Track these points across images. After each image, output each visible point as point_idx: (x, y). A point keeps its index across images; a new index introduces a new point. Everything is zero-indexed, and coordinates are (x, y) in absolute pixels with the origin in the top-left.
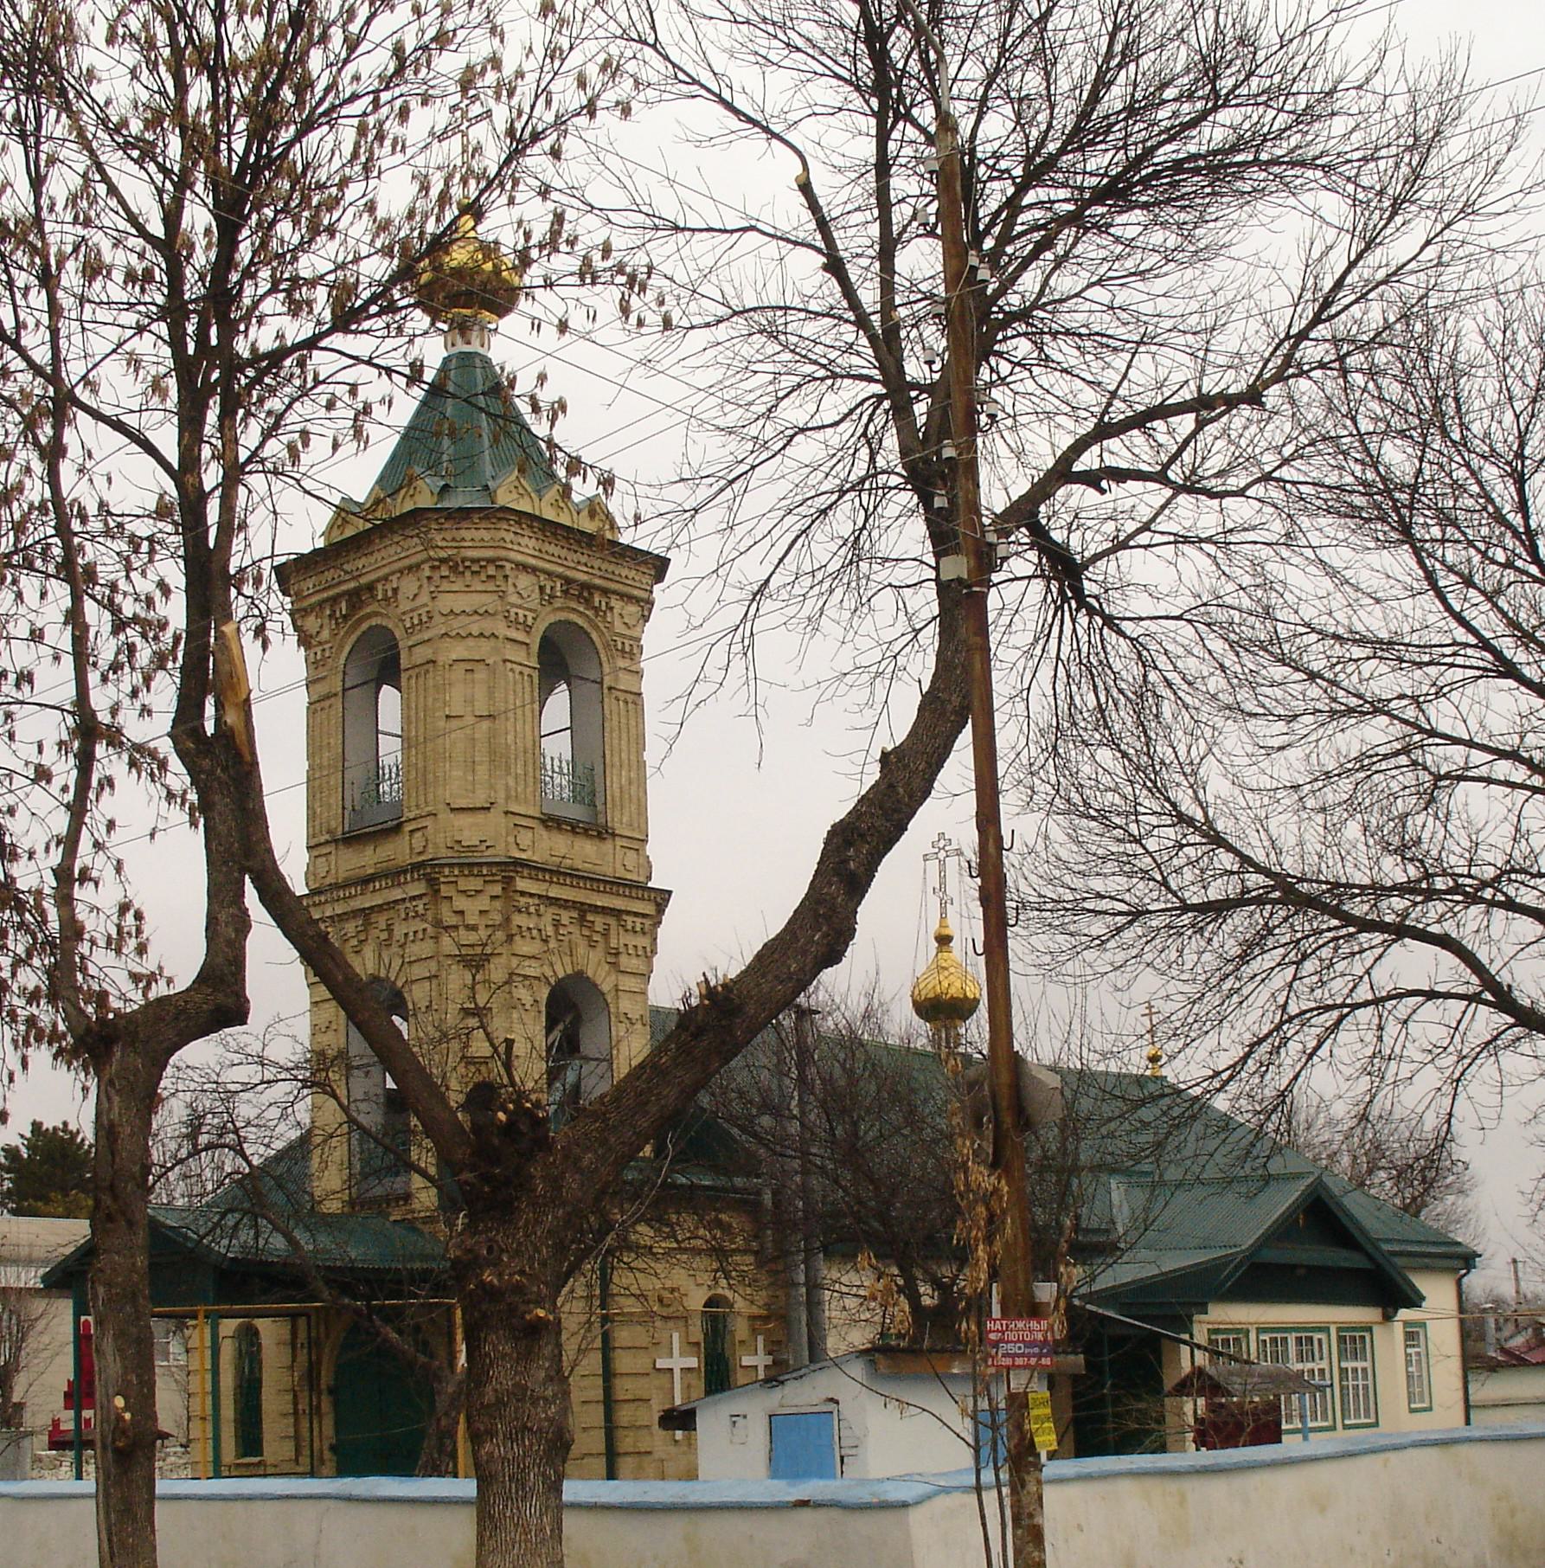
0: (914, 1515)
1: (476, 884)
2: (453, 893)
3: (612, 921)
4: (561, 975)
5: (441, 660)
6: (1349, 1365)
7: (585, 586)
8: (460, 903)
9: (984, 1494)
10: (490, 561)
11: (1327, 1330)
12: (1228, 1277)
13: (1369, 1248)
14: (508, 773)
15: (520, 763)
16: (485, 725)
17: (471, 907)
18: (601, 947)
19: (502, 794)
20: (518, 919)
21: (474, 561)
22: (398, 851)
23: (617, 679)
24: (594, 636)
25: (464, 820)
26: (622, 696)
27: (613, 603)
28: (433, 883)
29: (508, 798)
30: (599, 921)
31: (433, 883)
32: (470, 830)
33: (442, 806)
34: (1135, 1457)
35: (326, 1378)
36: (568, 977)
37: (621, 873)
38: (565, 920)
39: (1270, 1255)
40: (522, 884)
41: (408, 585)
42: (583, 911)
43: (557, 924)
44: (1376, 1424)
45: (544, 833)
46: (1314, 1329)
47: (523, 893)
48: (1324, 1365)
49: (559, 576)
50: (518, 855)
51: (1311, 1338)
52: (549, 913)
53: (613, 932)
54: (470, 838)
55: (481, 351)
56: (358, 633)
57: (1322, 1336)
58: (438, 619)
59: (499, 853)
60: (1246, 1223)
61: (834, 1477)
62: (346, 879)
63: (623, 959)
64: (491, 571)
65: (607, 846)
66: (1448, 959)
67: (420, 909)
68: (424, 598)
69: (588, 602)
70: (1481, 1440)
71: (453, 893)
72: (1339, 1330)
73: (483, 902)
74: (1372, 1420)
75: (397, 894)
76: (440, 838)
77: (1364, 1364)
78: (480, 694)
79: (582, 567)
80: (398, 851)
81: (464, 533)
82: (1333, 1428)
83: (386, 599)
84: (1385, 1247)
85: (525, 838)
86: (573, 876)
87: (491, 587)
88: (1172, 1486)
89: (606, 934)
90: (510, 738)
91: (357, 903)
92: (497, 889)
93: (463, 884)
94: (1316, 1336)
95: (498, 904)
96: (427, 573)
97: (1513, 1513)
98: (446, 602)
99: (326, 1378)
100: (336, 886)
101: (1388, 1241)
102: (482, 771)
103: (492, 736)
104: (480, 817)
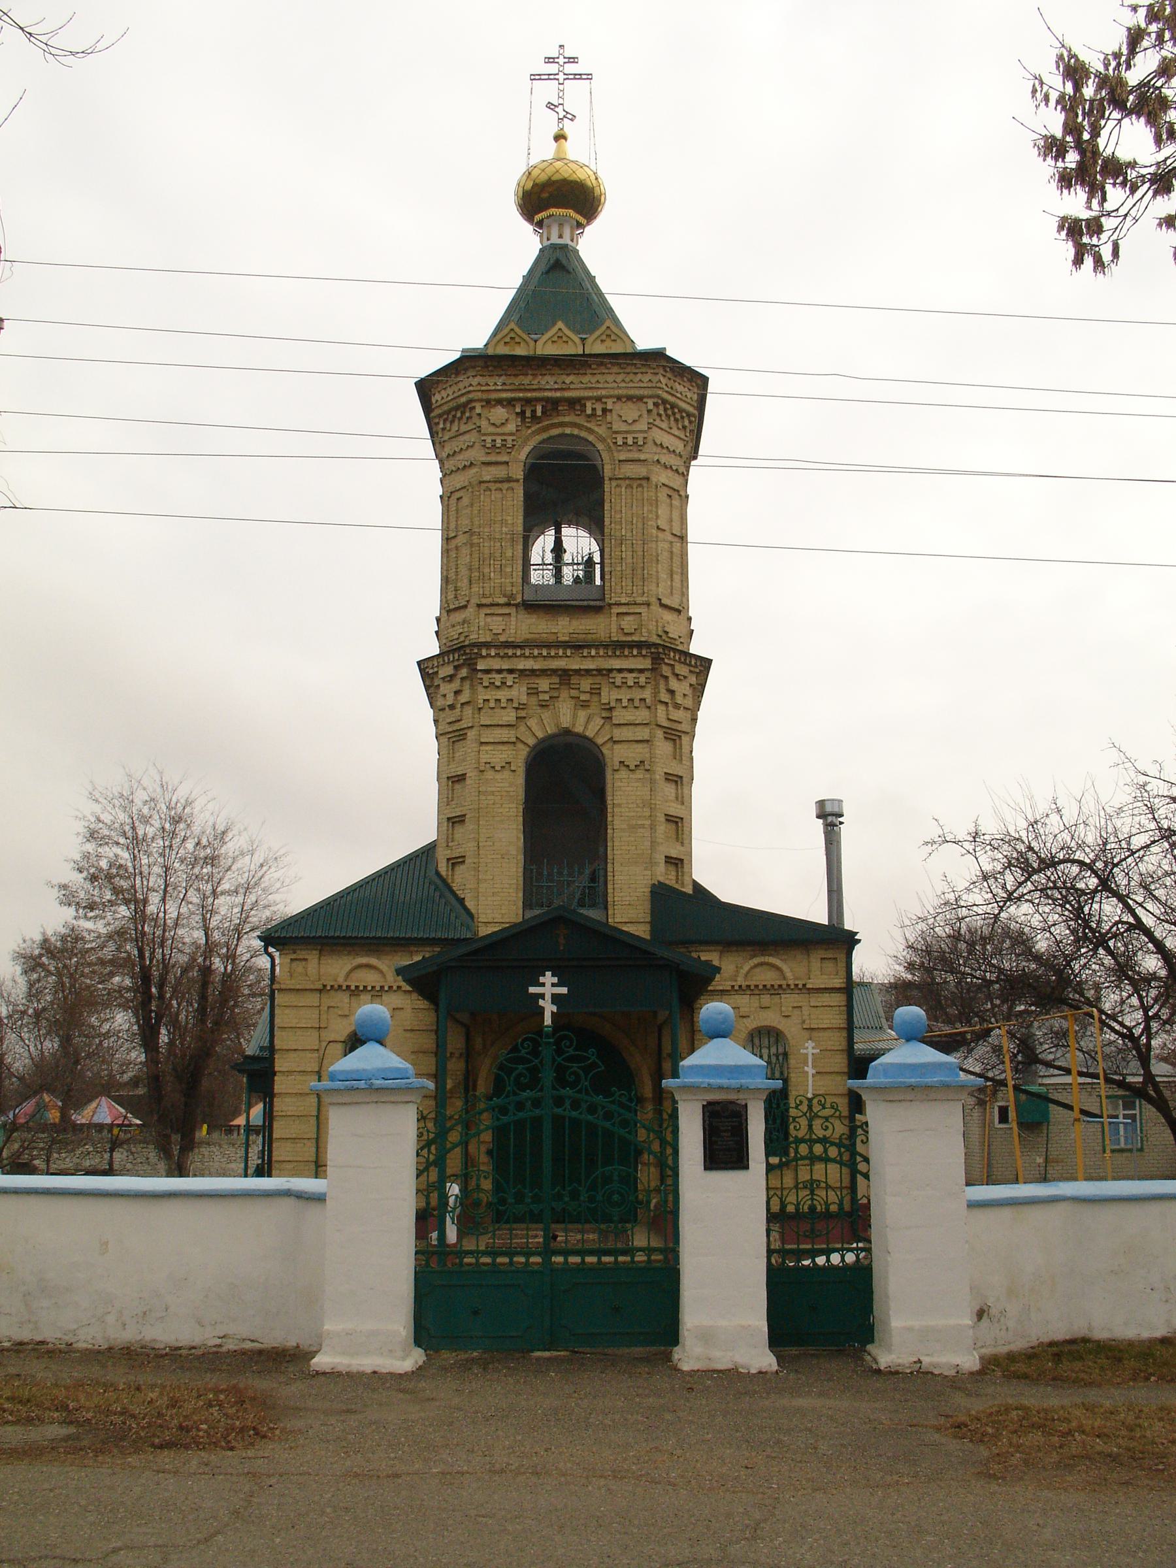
2: (669, 674)
5: (654, 479)
9: (314, 1159)
22: (600, 627)
28: (657, 660)
33: (653, 600)
34: (762, 1127)
35: (483, 1086)
41: (630, 411)
55: (570, 243)
56: (545, 436)
58: (650, 447)
62: (527, 640)
67: (642, 680)
71: (669, 674)
75: (617, 664)
76: (652, 626)
80: (600, 627)
81: (677, 386)
83: (594, 415)
87: (470, 426)
96: (651, 406)
99: (483, 1086)
100: (507, 645)
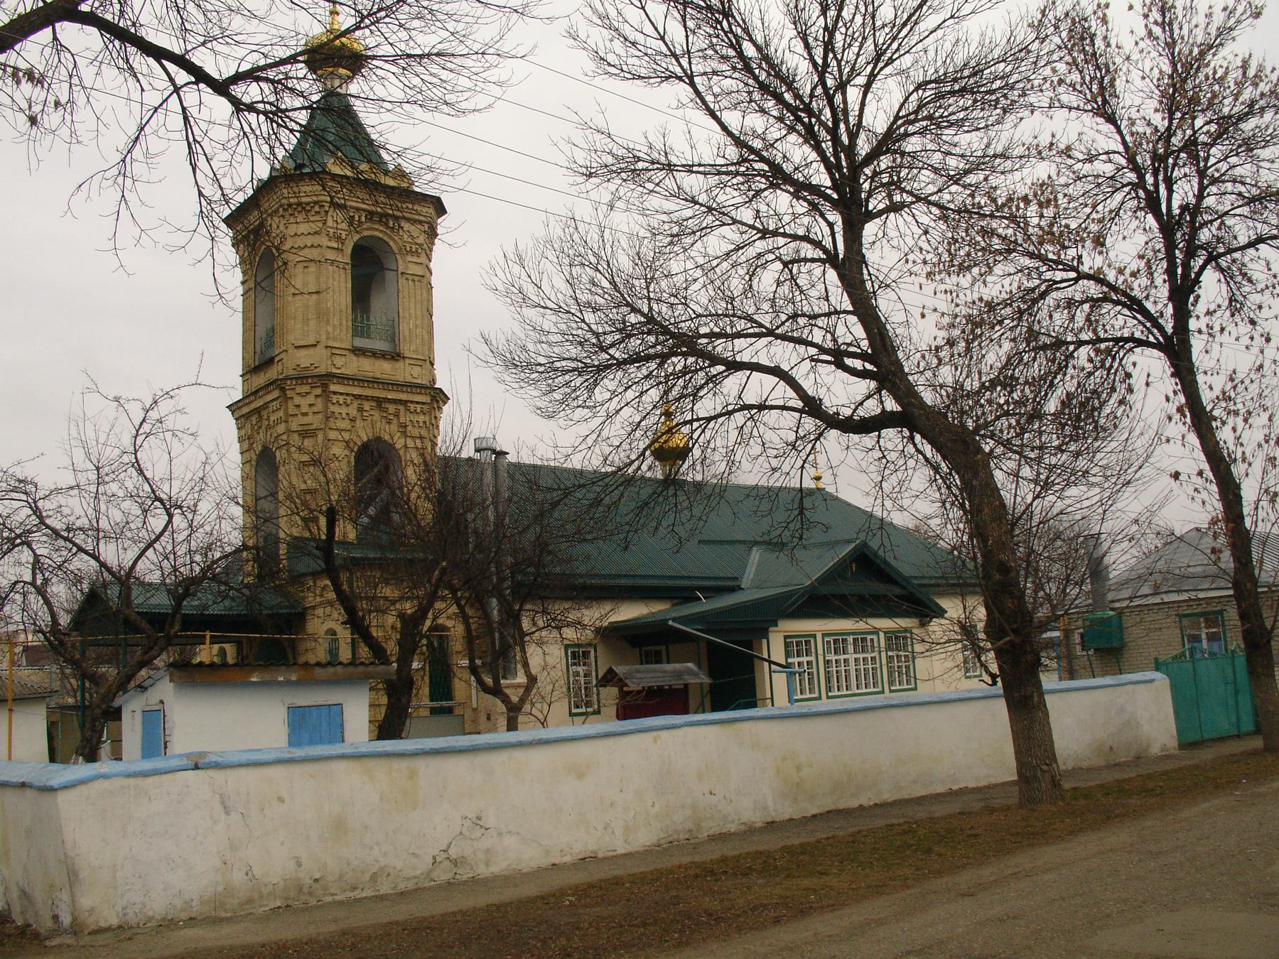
0: (62, 797)
1: (306, 389)
3: (402, 408)
4: (365, 439)
6: (861, 656)
7: (381, 215)
8: (297, 400)
10: (315, 203)
11: (814, 636)
12: (793, 604)
13: (904, 583)
14: (328, 323)
15: (338, 316)
16: (314, 297)
17: (304, 402)
18: (395, 421)
19: (324, 337)
20: (332, 408)
21: (308, 204)
23: (407, 268)
24: (391, 244)
25: (303, 352)
26: (410, 277)
27: (402, 224)
28: (283, 390)
29: (328, 338)
30: (392, 408)
31: (283, 390)
32: (304, 359)
36: (369, 440)
37: (409, 379)
38: (367, 408)
39: (825, 590)
40: (333, 388)
42: (380, 402)
43: (361, 410)
44: (915, 689)
45: (355, 358)
46: (849, 634)
47: (335, 393)
48: (812, 658)
49: (364, 210)
50: (334, 371)
51: (864, 640)
52: (356, 404)
53: (402, 413)
54: (305, 363)
57: (874, 637)
59: (322, 370)
60: (812, 567)
61: (159, 755)
63: (409, 428)
64: (317, 209)
65: (400, 365)
66: (771, 380)
68: (282, 228)
69: (386, 225)
70: (979, 698)
72: (824, 635)
73: (311, 399)
74: (816, 695)
77: (809, 659)
78: (311, 279)
79: (383, 204)
82: (883, 692)
84: (915, 582)
85: (339, 361)
86: (374, 382)
88: (404, 764)
89: (397, 415)
90: (330, 304)
91: (254, 406)
92: (318, 391)
93: (299, 389)
94: (869, 637)
95: (319, 400)
97: (799, 768)
98: (292, 229)
101: (916, 578)
102: (312, 323)
103: (318, 303)
104: (312, 351)
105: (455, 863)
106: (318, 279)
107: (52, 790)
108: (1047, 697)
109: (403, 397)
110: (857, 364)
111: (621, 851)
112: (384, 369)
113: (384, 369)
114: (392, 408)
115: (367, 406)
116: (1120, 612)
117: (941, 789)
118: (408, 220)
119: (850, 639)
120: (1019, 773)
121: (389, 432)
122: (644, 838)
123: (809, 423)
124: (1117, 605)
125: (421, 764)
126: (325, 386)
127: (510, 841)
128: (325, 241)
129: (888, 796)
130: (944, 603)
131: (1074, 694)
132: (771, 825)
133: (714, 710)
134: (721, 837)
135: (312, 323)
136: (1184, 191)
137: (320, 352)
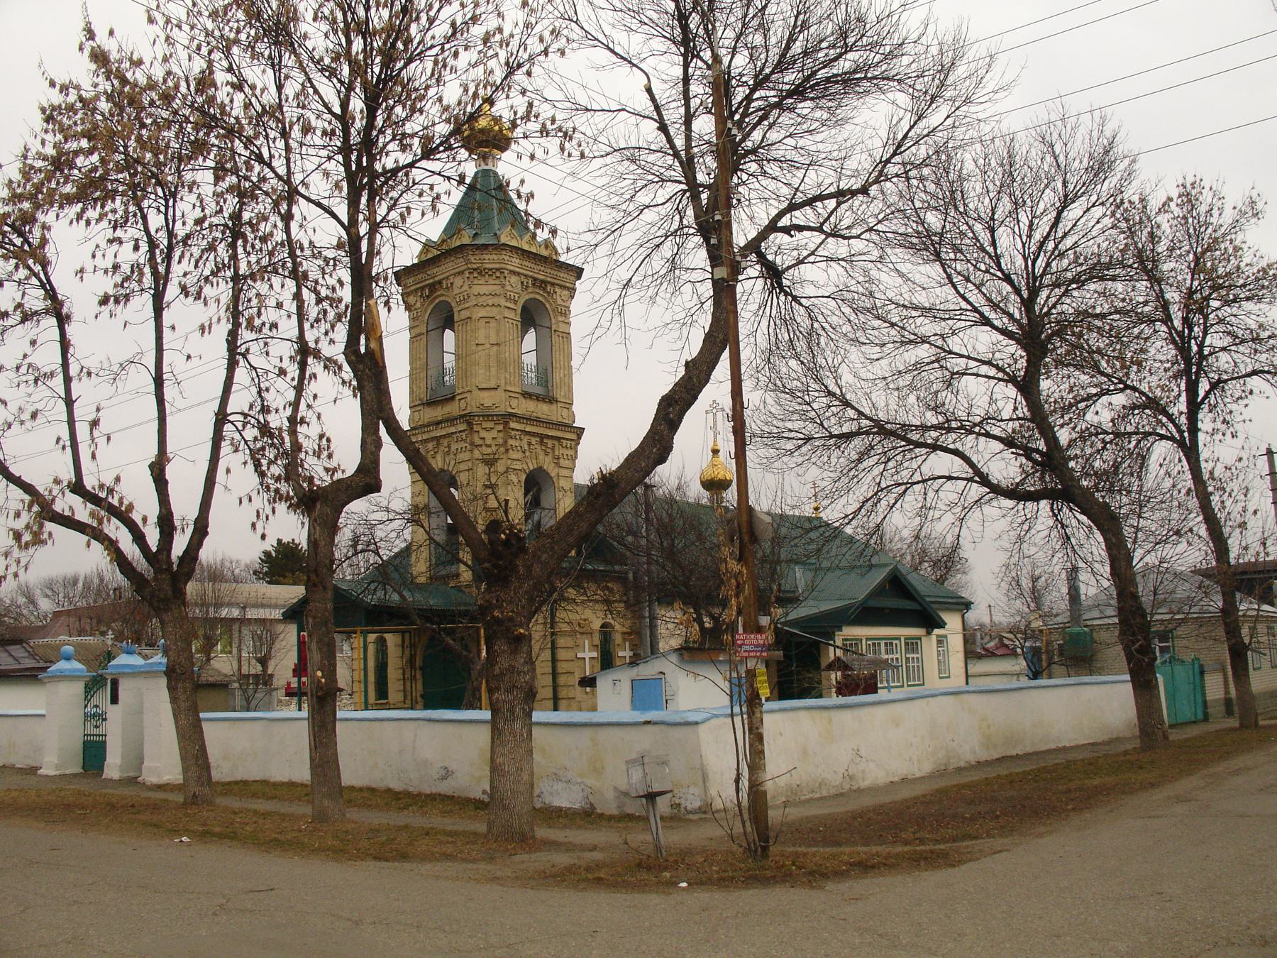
0: (702, 728)
1: (490, 425)
3: (556, 443)
6: (910, 656)
7: (543, 282)
8: (483, 434)
10: (498, 269)
16: (495, 348)
17: (488, 436)
20: (511, 442)
28: (470, 424)
31: (470, 424)
32: (487, 399)
39: (872, 603)
40: (512, 425)
42: (542, 437)
43: (530, 444)
54: (488, 403)
59: (502, 409)
60: (860, 588)
65: (554, 406)
68: (466, 287)
69: (544, 289)
73: (494, 433)
79: (542, 273)
85: (514, 403)
88: (825, 714)
89: (553, 449)
92: (501, 427)
95: (501, 434)
98: (476, 289)
102: (493, 370)
103: (498, 353)
104: (493, 393)
105: (851, 778)
106: (498, 332)
107: (697, 723)
108: (339, 727)
109: (559, 434)
110: (1038, 457)
111: (917, 776)
112: (542, 410)
113: (542, 410)
114: (550, 443)
115: (534, 440)
116: (1092, 628)
117: (1053, 746)
118: (561, 286)
119: (883, 643)
120: (1141, 730)
121: (547, 464)
122: (927, 768)
123: (976, 490)
124: (1089, 623)
125: (833, 714)
126: (506, 423)
127: (872, 765)
128: (503, 302)
129: (1029, 749)
130: (946, 617)
131: (1118, 685)
132: (980, 764)
133: (426, 707)
134: (959, 770)
135: (493, 370)
136: (358, 45)
137: (500, 394)
